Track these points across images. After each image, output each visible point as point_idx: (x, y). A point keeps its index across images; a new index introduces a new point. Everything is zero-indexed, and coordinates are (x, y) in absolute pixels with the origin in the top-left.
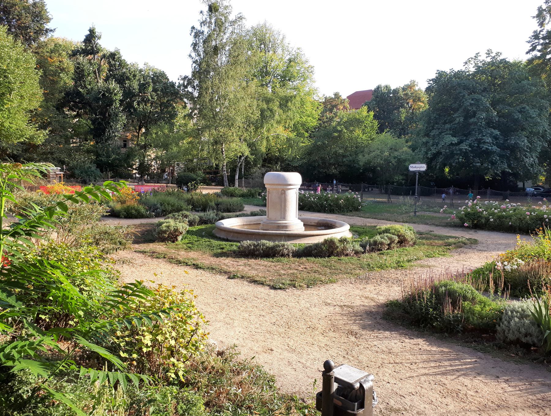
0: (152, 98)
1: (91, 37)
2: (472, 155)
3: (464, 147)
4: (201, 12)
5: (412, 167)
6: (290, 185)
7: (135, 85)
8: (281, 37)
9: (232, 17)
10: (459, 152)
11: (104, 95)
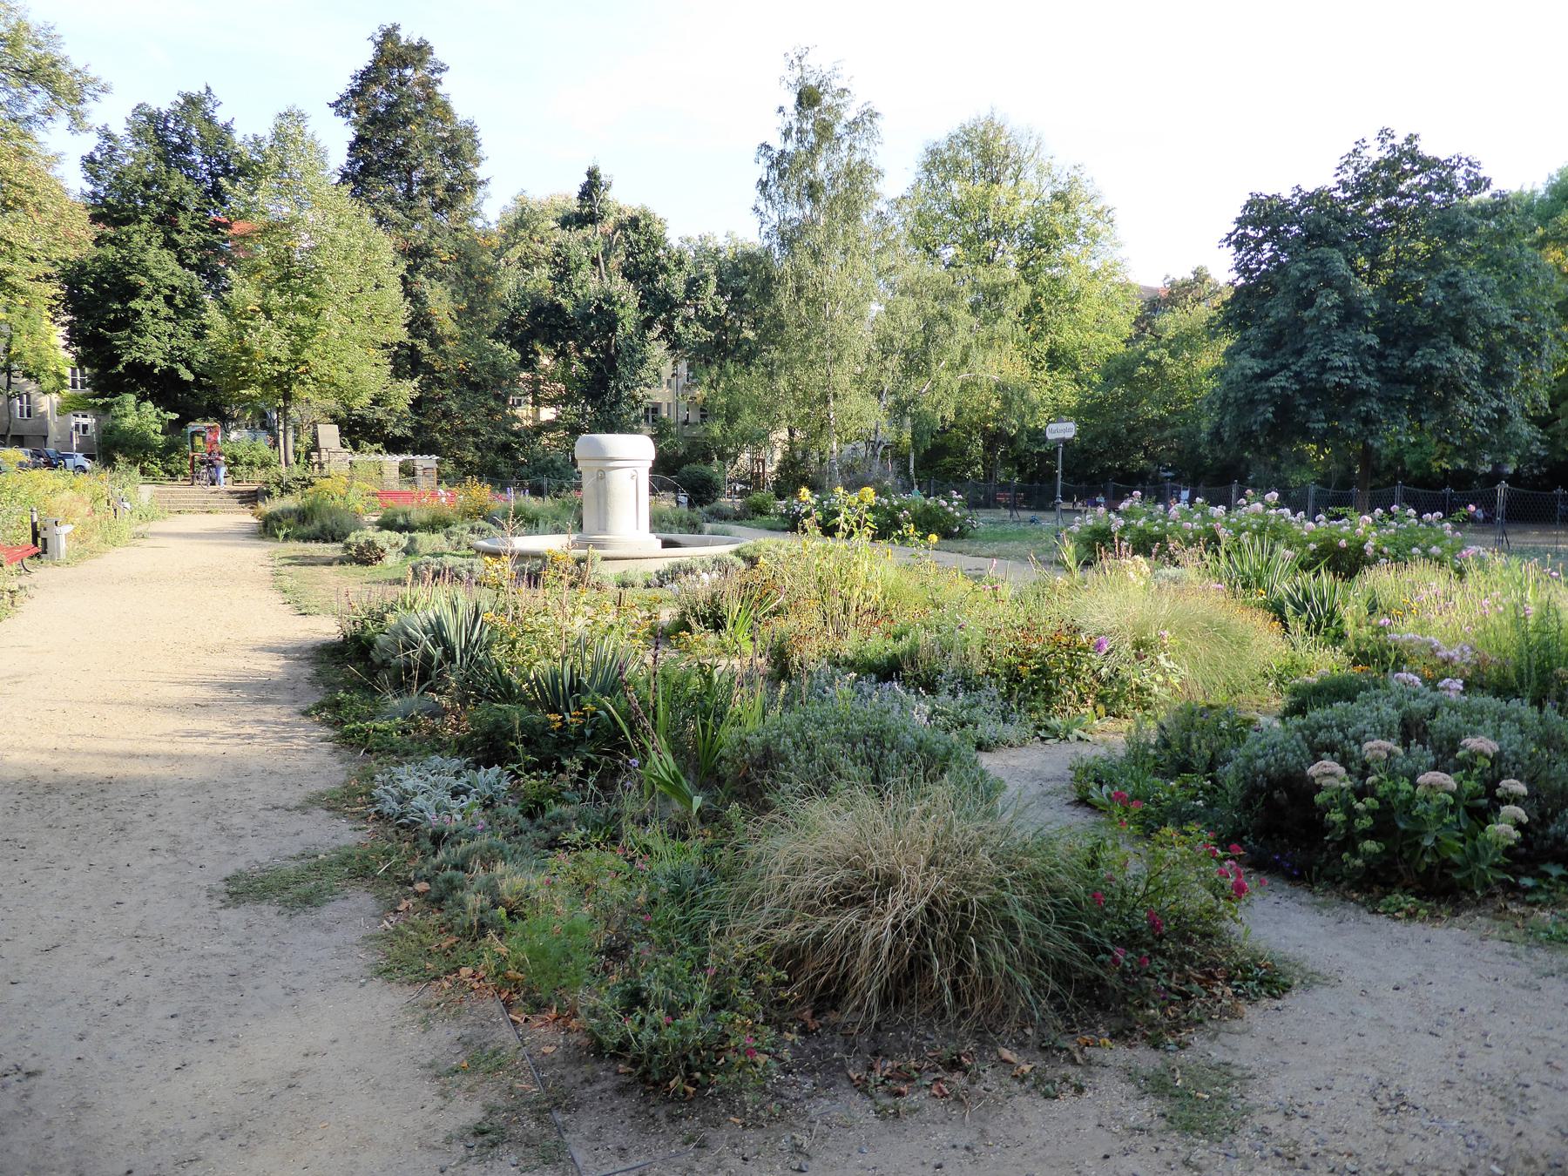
0: (716, 309)
1: (592, 186)
2: (1303, 402)
3: (1278, 382)
4: (781, 109)
5: (1070, 430)
6: (612, 460)
7: (678, 286)
8: (1033, 144)
9: (850, 115)
10: (1266, 396)
11: (599, 308)
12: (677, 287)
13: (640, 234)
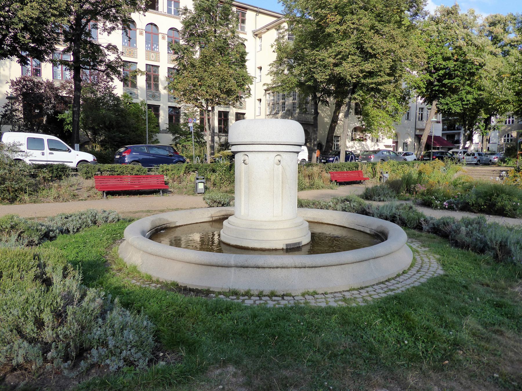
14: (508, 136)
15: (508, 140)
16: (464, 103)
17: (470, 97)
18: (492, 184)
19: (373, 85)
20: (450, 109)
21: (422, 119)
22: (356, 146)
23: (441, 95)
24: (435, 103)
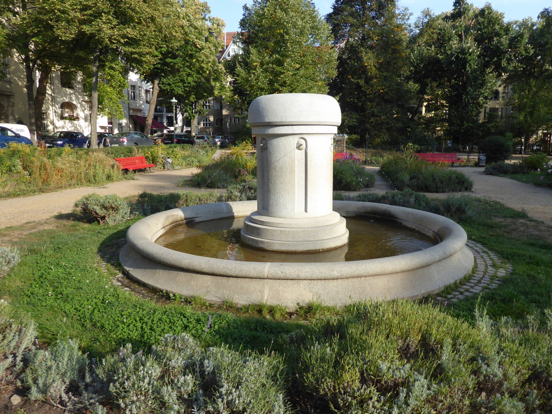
0: (526, 52)
12: (504, 43)
13: (485, 18)
14: (206, 121)
15: (207, 124)
16: (185, 85)
17: (190, 79)
18: (466, 177)
19: (136, 56)
20: (173, 90)
21: (134, 98)
22: (68, 126)
23: (163, 74)
24: (156, 82)
